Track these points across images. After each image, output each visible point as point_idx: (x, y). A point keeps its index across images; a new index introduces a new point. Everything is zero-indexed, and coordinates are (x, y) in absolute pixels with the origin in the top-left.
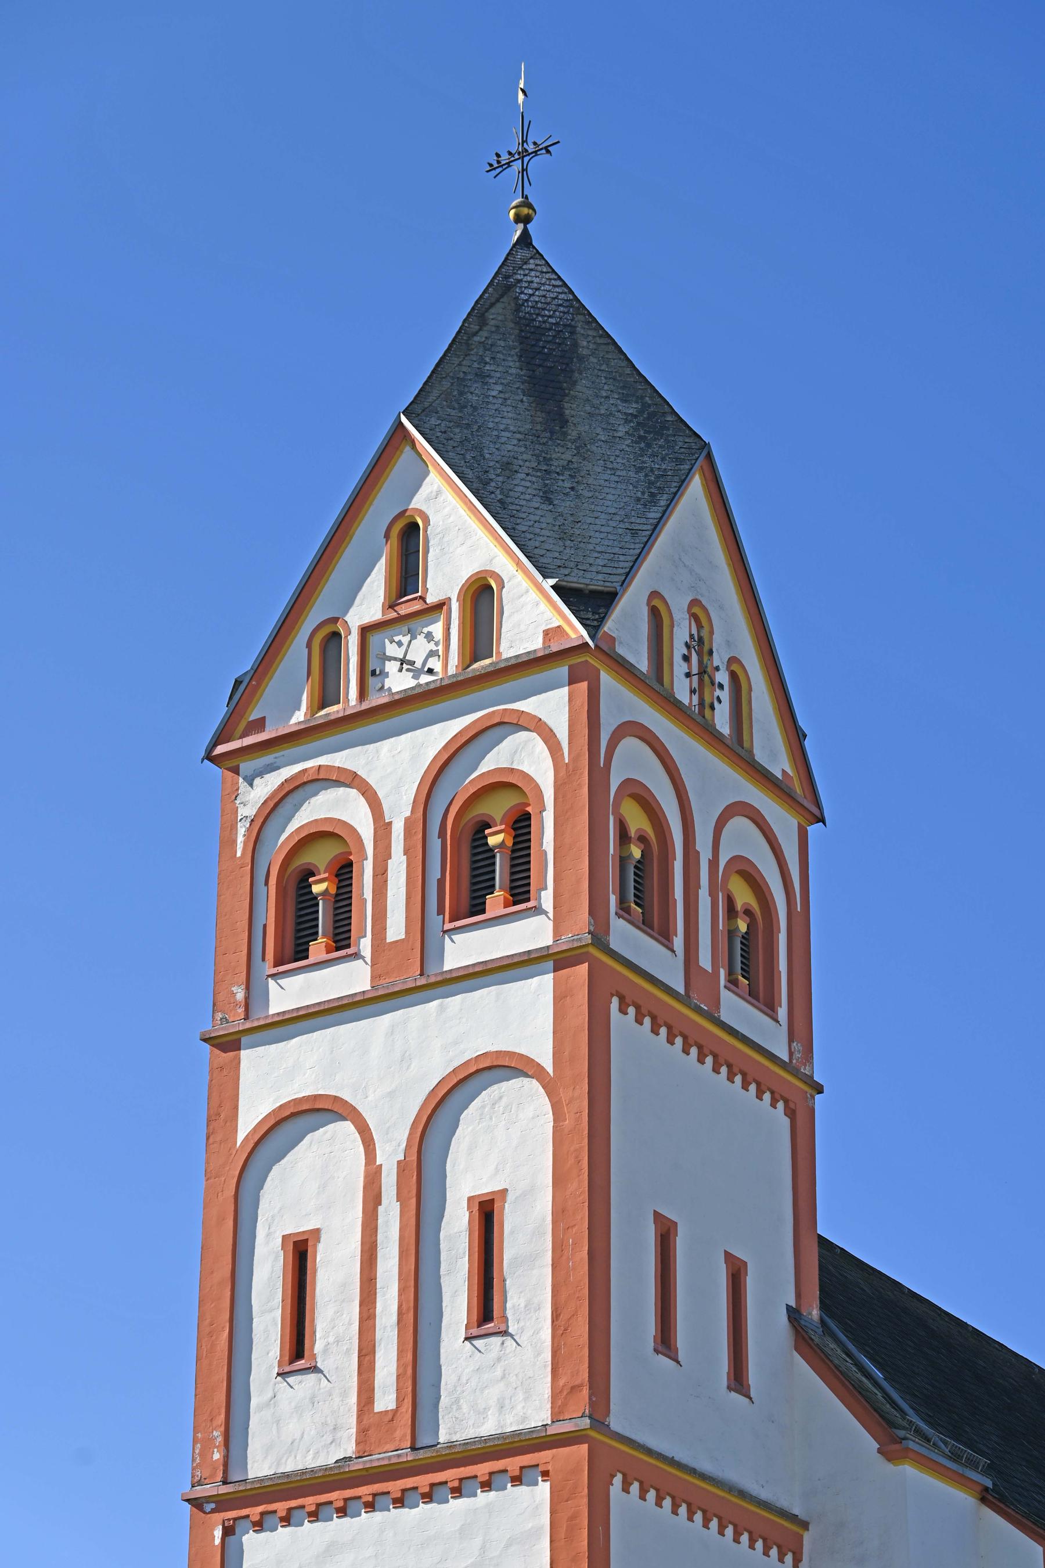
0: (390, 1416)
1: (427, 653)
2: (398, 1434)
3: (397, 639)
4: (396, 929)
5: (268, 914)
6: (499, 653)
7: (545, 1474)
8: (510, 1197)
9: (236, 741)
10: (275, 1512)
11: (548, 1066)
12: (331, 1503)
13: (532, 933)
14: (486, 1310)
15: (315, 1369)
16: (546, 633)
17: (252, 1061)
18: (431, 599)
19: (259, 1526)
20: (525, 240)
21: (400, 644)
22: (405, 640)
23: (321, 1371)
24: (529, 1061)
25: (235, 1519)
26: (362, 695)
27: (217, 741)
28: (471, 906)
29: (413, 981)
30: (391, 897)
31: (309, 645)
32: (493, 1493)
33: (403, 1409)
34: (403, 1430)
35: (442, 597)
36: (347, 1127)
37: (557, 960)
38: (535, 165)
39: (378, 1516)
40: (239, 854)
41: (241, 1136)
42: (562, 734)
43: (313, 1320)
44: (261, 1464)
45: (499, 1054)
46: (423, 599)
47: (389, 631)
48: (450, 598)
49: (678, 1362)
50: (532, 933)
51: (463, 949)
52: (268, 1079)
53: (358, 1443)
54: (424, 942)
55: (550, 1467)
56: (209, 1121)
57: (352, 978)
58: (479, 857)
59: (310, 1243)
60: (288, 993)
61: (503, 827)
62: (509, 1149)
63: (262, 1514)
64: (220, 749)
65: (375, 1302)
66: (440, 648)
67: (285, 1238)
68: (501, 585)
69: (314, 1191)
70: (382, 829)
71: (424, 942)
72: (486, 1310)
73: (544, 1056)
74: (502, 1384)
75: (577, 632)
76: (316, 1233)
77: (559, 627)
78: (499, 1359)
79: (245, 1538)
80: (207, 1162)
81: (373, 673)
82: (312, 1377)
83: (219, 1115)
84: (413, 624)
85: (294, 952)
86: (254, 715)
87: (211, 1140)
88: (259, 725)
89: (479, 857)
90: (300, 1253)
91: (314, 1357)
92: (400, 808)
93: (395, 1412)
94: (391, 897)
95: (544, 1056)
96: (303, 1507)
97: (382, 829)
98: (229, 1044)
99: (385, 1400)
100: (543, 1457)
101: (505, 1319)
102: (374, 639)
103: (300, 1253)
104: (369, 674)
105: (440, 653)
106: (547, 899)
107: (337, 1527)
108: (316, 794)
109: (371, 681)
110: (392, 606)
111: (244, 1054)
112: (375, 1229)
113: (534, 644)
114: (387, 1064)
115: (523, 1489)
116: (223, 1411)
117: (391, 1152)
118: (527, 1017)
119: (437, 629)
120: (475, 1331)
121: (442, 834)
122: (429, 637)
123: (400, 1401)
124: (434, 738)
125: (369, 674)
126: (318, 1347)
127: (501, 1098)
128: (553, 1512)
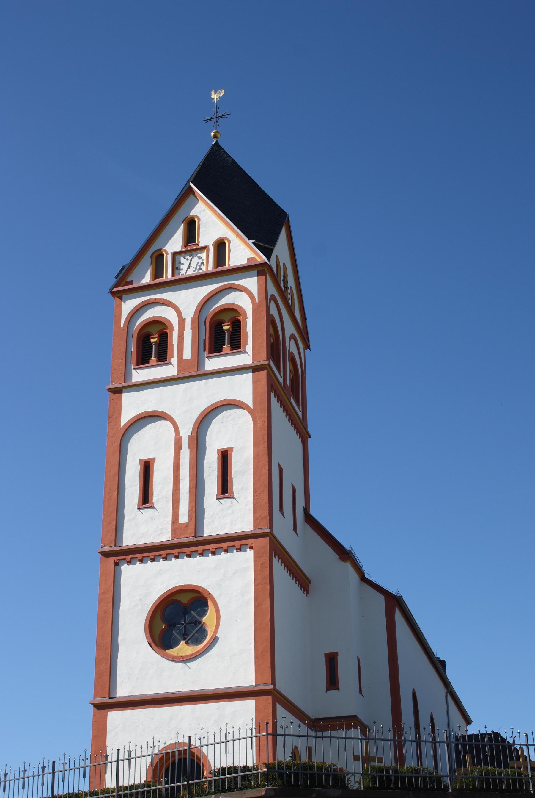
0: (186, 525)
1: (204, 262)
2: (189, 531)
3: (186, 257)
4: (187, 354)
5: (133, 348)
6: (229, 265)
7: (251, 548)
8: (234, 450)
9: (122, 285)
10: (137, 558)
11: (251, 405)
12: (161, 555)
13: (245, 359)
14: (225, 488)
15: (152, 507)
16: (248, 259)
17: (126, 397)
18: (201, 245)
19: (129, 563)
20: (217, 143)
21: (187, 259)
22: (189, 258)
23: (155, 508)
24: (243, 403)
25: (119, 560)
26: (173, 275)
27: (117, 285)
28: (216, 348)
29: (192, 373)
30: (184, 344)
31: (151, 257)
32: (228, 554)
33: (191, 523)
34: (191, 530)
35: (206, 245)
36: (167, 424)
37: (255, 369)
38: (221, 120)
39: (180, 561)
40: (122, 326)
41: (122, 424)
42: (255, 292)
43: (152, 490)
44: (129, 540)
45: (230, 400)
46: (198, 245)
47: (184, 255)
48: (208, 246)
49: (283, 515)
50: (245, 359)
51: (212, 364)
52: (132, 405)
53: (172, 534)
54: (198, 360)
55: (253, 545)
56: (109, 418)
57: (169, 370)
58: (220, 332)
59: (151, 463)
60: (139, 375)
61: (229, 323)
62: (235, 433)
63: (131, 558)
64: (115, 289)
65: (179, 484)
66: (205, 262)
67: (140, 461)
68: (229, 242)
69: (151, 444)
70: (182, 322)
71: (198, 360)
72: (225, 488)
73: (250, 402)
74: (234, 514)
75: (261, 258)
76: (153, 459)
77: (253, 257)
78: (230, 507)
79: (122, 567)
80: (108, 432)
81: (177, 268)
82: (151, 510)
83: (113, 416)
84: (193, 253)
85: (143, 360)
86: (129, 279)
87: (110, 424)
88: (131, 283)
89: (220, 332)
90: (147, 467)
91: (153, 503)
92: (189, 314)
93: (188, 524)
94: (184, 344)
95: (250, 402)
96: (149, 556)
97: (182, 322)
98: (118, 391)
99: (184, 518)
100: (251, 541)
101: (233, 493)
102: (177, 257)
103: (147, 467)
104: (175, 268)
105: (205, 263)
106: (249, 348)
107: (162, 563)
108: (153, 307)
109: (176, 271)
110: (185, 246)
111: (124, 395)
112: (179, 459)
113: (243, 262)
114: (185, 402)
115: (240, 553)
116: (115, 521)
117: (186, 432)
118: (243, 388)
119: (203, 255)
120: (220, 496)
121: (205, 324)
122: (200, 258)
123: (190, 519)
124: (203, 291)
125: (175, 268)
126: (154, 500)
127: (230, 415)
128: (255, 561)
